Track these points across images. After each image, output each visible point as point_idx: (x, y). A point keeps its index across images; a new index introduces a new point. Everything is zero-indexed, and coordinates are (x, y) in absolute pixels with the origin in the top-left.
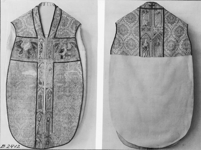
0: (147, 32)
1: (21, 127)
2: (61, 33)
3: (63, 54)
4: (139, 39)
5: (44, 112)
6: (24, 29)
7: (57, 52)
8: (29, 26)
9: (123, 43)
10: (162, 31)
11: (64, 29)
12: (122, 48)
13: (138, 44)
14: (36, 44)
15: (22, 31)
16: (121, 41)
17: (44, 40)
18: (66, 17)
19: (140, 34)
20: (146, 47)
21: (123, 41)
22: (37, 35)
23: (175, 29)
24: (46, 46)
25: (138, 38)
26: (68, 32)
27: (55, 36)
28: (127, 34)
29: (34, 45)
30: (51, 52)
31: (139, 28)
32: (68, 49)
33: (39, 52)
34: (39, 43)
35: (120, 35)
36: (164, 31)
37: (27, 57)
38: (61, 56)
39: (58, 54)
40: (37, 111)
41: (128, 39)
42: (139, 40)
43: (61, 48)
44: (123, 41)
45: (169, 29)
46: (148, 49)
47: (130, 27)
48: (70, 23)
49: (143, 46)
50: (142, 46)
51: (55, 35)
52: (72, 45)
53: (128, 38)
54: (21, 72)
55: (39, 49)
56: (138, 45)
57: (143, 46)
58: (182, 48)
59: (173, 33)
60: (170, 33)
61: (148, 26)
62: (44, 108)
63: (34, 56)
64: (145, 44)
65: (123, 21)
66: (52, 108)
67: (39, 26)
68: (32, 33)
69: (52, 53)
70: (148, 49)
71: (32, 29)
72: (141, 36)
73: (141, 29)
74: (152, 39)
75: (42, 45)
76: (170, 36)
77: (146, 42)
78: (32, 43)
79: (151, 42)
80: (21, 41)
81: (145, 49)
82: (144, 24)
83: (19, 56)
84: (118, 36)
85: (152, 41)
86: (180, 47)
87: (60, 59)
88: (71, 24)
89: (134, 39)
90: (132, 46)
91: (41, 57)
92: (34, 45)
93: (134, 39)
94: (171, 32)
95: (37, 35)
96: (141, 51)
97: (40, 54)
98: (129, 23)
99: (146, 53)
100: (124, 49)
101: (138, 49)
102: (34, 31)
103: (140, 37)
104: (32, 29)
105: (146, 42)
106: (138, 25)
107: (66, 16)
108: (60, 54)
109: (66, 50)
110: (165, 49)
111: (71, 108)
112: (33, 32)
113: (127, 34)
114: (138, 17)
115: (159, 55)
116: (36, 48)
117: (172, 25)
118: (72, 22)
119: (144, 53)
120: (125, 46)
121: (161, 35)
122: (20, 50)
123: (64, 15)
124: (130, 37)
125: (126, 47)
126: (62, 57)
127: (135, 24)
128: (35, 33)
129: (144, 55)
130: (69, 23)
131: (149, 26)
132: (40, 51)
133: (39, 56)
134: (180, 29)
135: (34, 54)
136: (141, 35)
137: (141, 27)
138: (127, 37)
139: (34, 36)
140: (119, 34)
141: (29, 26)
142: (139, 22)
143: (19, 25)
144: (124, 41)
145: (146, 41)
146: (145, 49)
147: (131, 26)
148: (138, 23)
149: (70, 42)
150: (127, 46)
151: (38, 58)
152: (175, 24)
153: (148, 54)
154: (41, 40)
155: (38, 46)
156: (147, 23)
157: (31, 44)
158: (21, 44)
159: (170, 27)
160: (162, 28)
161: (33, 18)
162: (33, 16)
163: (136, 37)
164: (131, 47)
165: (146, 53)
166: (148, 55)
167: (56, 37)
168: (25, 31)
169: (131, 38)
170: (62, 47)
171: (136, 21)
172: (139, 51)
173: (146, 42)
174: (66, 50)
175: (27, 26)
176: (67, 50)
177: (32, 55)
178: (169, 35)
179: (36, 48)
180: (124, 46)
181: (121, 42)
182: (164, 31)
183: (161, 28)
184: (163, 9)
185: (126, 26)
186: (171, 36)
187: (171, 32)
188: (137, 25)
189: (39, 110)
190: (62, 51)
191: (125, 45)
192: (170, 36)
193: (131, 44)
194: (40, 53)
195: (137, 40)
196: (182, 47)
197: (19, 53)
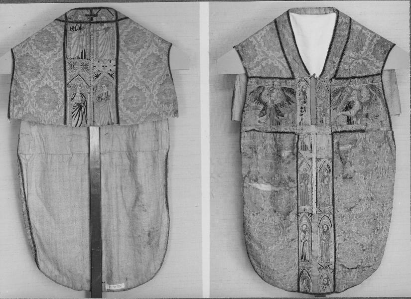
0: (81, 73)
2: (350, 67)
3: (352, 113)
4: (63, 88)
5: (314, 211)
6: (262, 60)
7: (338, 109)
8: (271, 53)
10: (114, 68)
11: (358, 58)
13: (61, 99)
14: (292, 91)
15: (258, 64)
17: (309, 81)
18: (361, 30)
19: (65, 75)
20: (80, 107)
22: (292, 73)
23: (141, 61)
24: (315, 96)
26: (366, 63)
27: (335, 75)
28: (36, 76)
29: (290, 96)
30: (325, 110)
31: (62, 64)
32: (362, 101)
33: (299, 109)
34: (298, 90)
36: (117, 68)
37: (275, 122)
38: (348, 117)
39: (340, 113)
40: (300, 211)
43: (346, 100)
45: (128, 64)
46: (83, 109)
47: (43, 61)
48: (370, 44)
49: (73, 103)
51: (336, 72)
52: (370, 91)
53: (40, 84)
55: (299, 104)
58: (159, 102)
59: (138, 71)
60: (130, 72)
61: (82, 58)
62: (314, 204)
63: (290, 118)
64: (78, 99)
65: (28, 46)
66: (331, 204)
67: (293, 50)
68: (281, 67)
69: (328, 112)
70: (83, 109)
71: (278, 59)
72: (67, 82)
73: (68, 66)
74: (92, 88)
75: (304, 94)
76: (131, 79)
77: (78, 94)
78: (283, 89)
79: (89, 93)
80: (260, 87)
81: (78, 110)
82: (75, 55)
83: (259, 122)
85: (92, 91)
86: (156, 100)
87: (346, 124)
88: (373, 47)
90: (49, 103)
91: (303, 121)
92: (289, 95)
94: (134, 69)
95: (292, 73)
97: (302, 115)
98: (42, 53)
99: (79, 116)
100: (31, 107)
102: (285, 64)
103: (65, 83)
104: (278, 59)
105: (79, 95)
106: (62, 56)
107: (360, 28)
108: (344, 113)
109: (357, 104)
110: (122, 107)
111: (372, 199)
112: (283, 65)
113: (36, 76)
115: (107, 121)
116: (292, 102)
117: (135, 53)
118: (375, 41)
120: (34, 101)
121: (111, 76)
122: (262, 107)
123: (357, 26)
126: (349, 120)
127: (55, 55)
128: (287, 68)
129: (74, 123)
130: (367, 44)
131: (85, 58)
132: (302, 108)
133: (298, 120)
134: (153, 60)
135: (290, 115)
137: (68, 61)
139: (286, 74)
141: (271, 53)
143: (249, 51)
144: (31, 90)
145: (78, 91)
146: (78, 110)
147: (46, 58)
148: (62, 52)
149: (366, 85)
151: (298, 124)
152: (141, 50)
153: (84, 118)
154: (302, 84)
155: (298, 97)
156: (81, 51)
157: (281, 92)
158: (261, 94)
159: (132, 59)
160: (114, 62)
161: (278, 33)
162: (277, 30)
165: (79, 116)
166: (84, 121)
167: (338, 76)
168: (264, 65)
169: (47, 85)
170: (349, 96)
171: (58, 42)
172: (63, 114)
173: (78, 94)
174: (357, 104)
175: (267, 52)
176: (361, 103)
177: (286, 115)
178: (129, 77)
179: (292, 102)
180: (31, 102)
182: (117, 68)
183: (110, 62)
184: (338, 11)
185: (35, 59)
186: (134, 78)
187: (134, 69)
188: (58, 57)
189: (303, 207)
190: (349, 107)
192: (131, 79)
194: (301, 111)
195: (59, 88)
196: (158, 100)
197: (259, 115)
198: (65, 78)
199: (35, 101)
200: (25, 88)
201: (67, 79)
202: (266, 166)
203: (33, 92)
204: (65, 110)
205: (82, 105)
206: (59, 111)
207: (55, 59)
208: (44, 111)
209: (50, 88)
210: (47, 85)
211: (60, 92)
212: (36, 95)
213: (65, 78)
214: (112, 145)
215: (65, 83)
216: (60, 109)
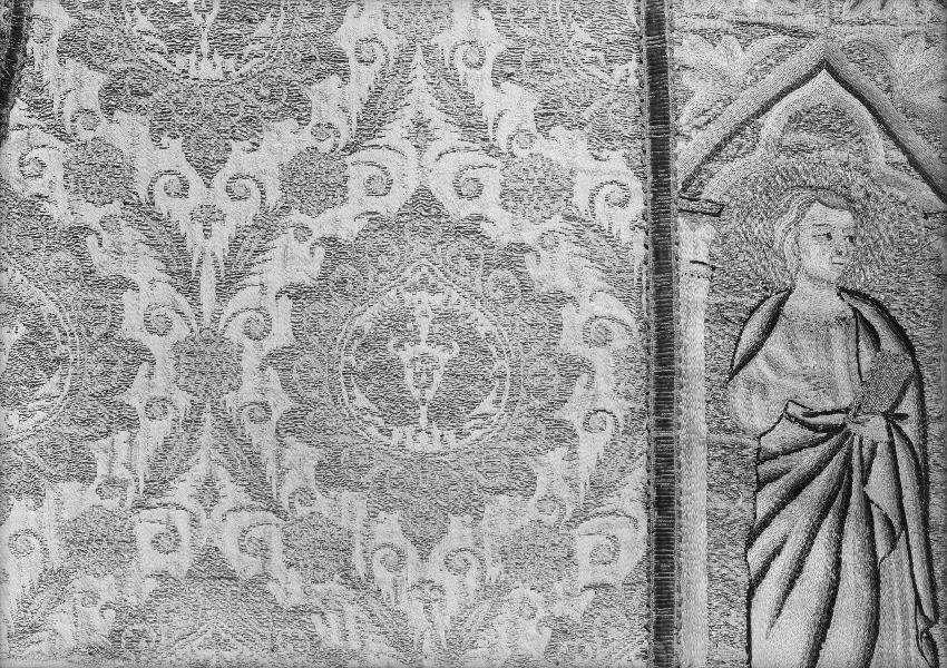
1: (209, 216)
4: (626, 221)
9: (180, 330)
12: (156, 486)
13: (600, 359)
16: (133, 309)
21: (187, 284)
25: (609, 184)
28: (296, 106)
35: (126, 132)
41: (344, 221)
42: (639, 252)
44: (187, 284)
50: (716, 400)
53: (334, 192)
54: (19, 96)
56: (609, 387)
57: (754, 412)
72: (686, 153)
84: (54, 155)
89: (490, 203)
93: (501, 227)
96: (695, 537)
101: (599, 488)
103: (660, 161)
105: (834, 305)
113: (296, 106)
114: (621, 341)
119: (769, 590)
124: (380, 185)
125: (262, 438)
136: (694, 94)
138: (311, 183)
140: (91, 95)
142: (639, 474)
144: (228, 285)
148: (631, 495)
150: (292, 425)
163: (565, 149)
164: (423, 440)
172: (634, 541)
181: (132, 327)
191: (248, 391)
193: (425, 361)
198: (659, 109)
199: (281, 404)
200: (146, 270)
201: (684, 117)
202: (693, 229)
203: (246, 297)
204: (663, 502)
205: (874, 429)
206: (581, 516)
207: (321, 225)
208: (389, 527)
209: (471, 229)
210: (424, 202)
211: (592, 278)
212: (281, 335)
213: (659, 109)
214: (757, 474)
215: (660, 161)
216: (599, 488)
